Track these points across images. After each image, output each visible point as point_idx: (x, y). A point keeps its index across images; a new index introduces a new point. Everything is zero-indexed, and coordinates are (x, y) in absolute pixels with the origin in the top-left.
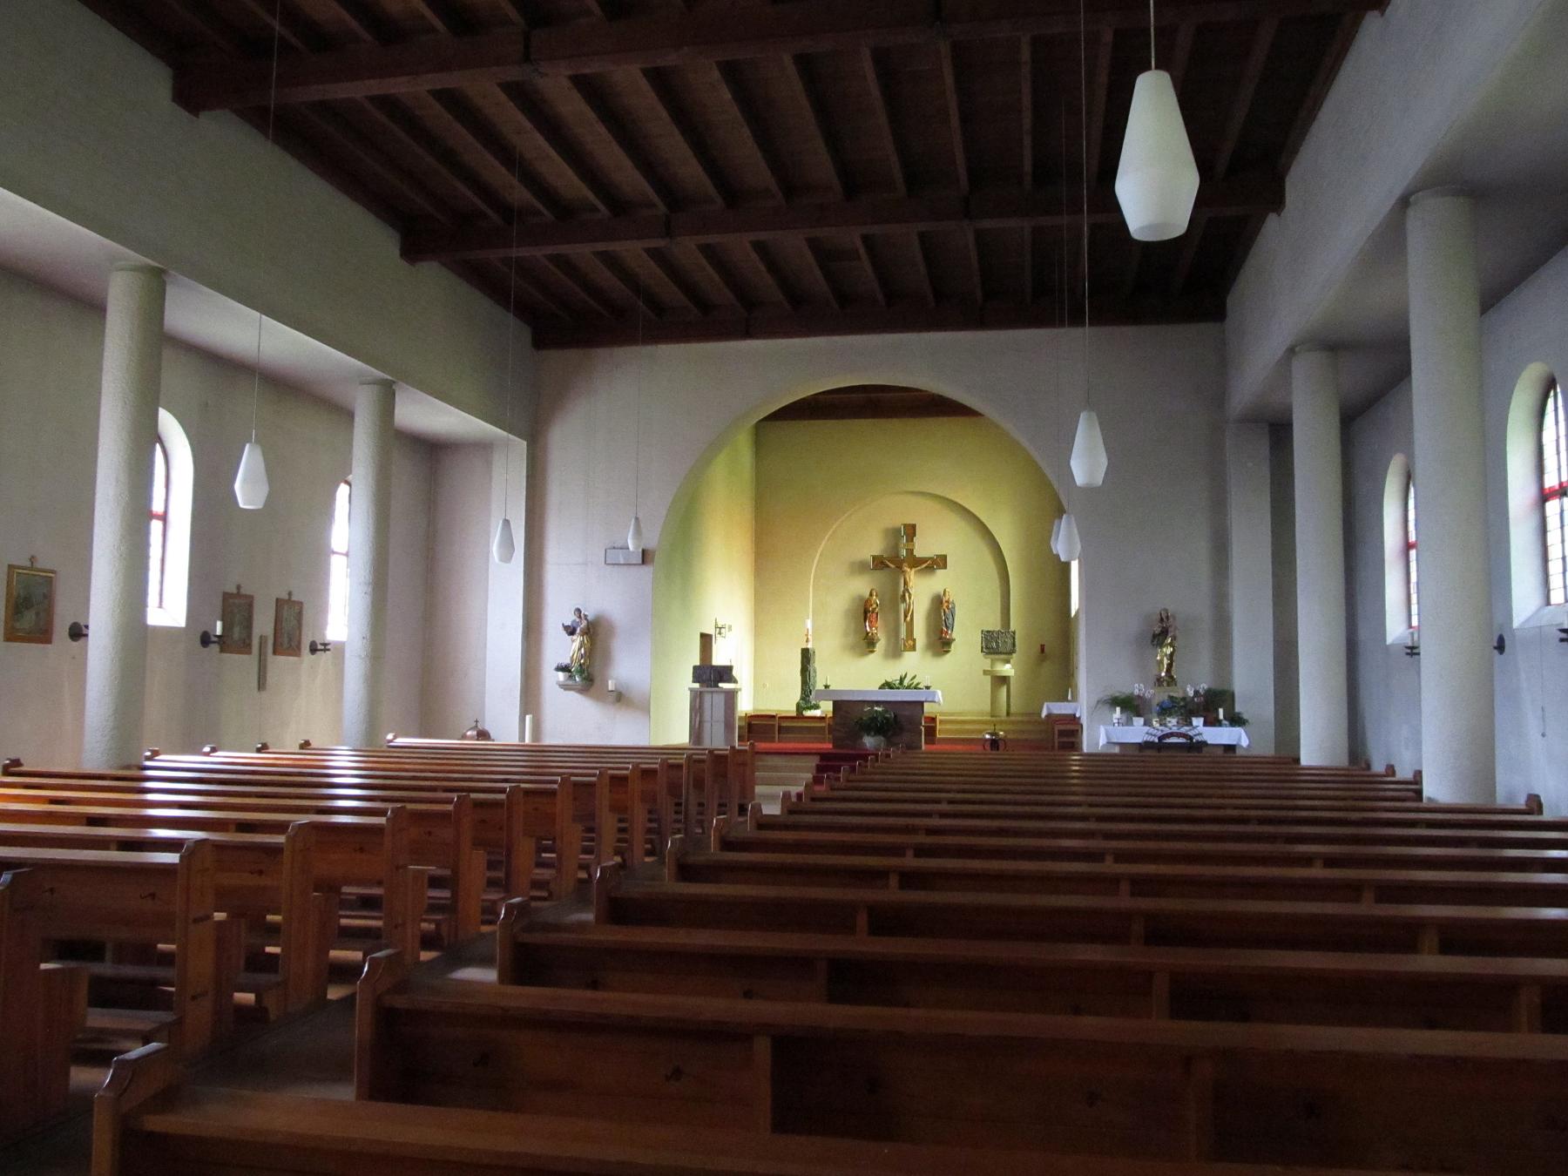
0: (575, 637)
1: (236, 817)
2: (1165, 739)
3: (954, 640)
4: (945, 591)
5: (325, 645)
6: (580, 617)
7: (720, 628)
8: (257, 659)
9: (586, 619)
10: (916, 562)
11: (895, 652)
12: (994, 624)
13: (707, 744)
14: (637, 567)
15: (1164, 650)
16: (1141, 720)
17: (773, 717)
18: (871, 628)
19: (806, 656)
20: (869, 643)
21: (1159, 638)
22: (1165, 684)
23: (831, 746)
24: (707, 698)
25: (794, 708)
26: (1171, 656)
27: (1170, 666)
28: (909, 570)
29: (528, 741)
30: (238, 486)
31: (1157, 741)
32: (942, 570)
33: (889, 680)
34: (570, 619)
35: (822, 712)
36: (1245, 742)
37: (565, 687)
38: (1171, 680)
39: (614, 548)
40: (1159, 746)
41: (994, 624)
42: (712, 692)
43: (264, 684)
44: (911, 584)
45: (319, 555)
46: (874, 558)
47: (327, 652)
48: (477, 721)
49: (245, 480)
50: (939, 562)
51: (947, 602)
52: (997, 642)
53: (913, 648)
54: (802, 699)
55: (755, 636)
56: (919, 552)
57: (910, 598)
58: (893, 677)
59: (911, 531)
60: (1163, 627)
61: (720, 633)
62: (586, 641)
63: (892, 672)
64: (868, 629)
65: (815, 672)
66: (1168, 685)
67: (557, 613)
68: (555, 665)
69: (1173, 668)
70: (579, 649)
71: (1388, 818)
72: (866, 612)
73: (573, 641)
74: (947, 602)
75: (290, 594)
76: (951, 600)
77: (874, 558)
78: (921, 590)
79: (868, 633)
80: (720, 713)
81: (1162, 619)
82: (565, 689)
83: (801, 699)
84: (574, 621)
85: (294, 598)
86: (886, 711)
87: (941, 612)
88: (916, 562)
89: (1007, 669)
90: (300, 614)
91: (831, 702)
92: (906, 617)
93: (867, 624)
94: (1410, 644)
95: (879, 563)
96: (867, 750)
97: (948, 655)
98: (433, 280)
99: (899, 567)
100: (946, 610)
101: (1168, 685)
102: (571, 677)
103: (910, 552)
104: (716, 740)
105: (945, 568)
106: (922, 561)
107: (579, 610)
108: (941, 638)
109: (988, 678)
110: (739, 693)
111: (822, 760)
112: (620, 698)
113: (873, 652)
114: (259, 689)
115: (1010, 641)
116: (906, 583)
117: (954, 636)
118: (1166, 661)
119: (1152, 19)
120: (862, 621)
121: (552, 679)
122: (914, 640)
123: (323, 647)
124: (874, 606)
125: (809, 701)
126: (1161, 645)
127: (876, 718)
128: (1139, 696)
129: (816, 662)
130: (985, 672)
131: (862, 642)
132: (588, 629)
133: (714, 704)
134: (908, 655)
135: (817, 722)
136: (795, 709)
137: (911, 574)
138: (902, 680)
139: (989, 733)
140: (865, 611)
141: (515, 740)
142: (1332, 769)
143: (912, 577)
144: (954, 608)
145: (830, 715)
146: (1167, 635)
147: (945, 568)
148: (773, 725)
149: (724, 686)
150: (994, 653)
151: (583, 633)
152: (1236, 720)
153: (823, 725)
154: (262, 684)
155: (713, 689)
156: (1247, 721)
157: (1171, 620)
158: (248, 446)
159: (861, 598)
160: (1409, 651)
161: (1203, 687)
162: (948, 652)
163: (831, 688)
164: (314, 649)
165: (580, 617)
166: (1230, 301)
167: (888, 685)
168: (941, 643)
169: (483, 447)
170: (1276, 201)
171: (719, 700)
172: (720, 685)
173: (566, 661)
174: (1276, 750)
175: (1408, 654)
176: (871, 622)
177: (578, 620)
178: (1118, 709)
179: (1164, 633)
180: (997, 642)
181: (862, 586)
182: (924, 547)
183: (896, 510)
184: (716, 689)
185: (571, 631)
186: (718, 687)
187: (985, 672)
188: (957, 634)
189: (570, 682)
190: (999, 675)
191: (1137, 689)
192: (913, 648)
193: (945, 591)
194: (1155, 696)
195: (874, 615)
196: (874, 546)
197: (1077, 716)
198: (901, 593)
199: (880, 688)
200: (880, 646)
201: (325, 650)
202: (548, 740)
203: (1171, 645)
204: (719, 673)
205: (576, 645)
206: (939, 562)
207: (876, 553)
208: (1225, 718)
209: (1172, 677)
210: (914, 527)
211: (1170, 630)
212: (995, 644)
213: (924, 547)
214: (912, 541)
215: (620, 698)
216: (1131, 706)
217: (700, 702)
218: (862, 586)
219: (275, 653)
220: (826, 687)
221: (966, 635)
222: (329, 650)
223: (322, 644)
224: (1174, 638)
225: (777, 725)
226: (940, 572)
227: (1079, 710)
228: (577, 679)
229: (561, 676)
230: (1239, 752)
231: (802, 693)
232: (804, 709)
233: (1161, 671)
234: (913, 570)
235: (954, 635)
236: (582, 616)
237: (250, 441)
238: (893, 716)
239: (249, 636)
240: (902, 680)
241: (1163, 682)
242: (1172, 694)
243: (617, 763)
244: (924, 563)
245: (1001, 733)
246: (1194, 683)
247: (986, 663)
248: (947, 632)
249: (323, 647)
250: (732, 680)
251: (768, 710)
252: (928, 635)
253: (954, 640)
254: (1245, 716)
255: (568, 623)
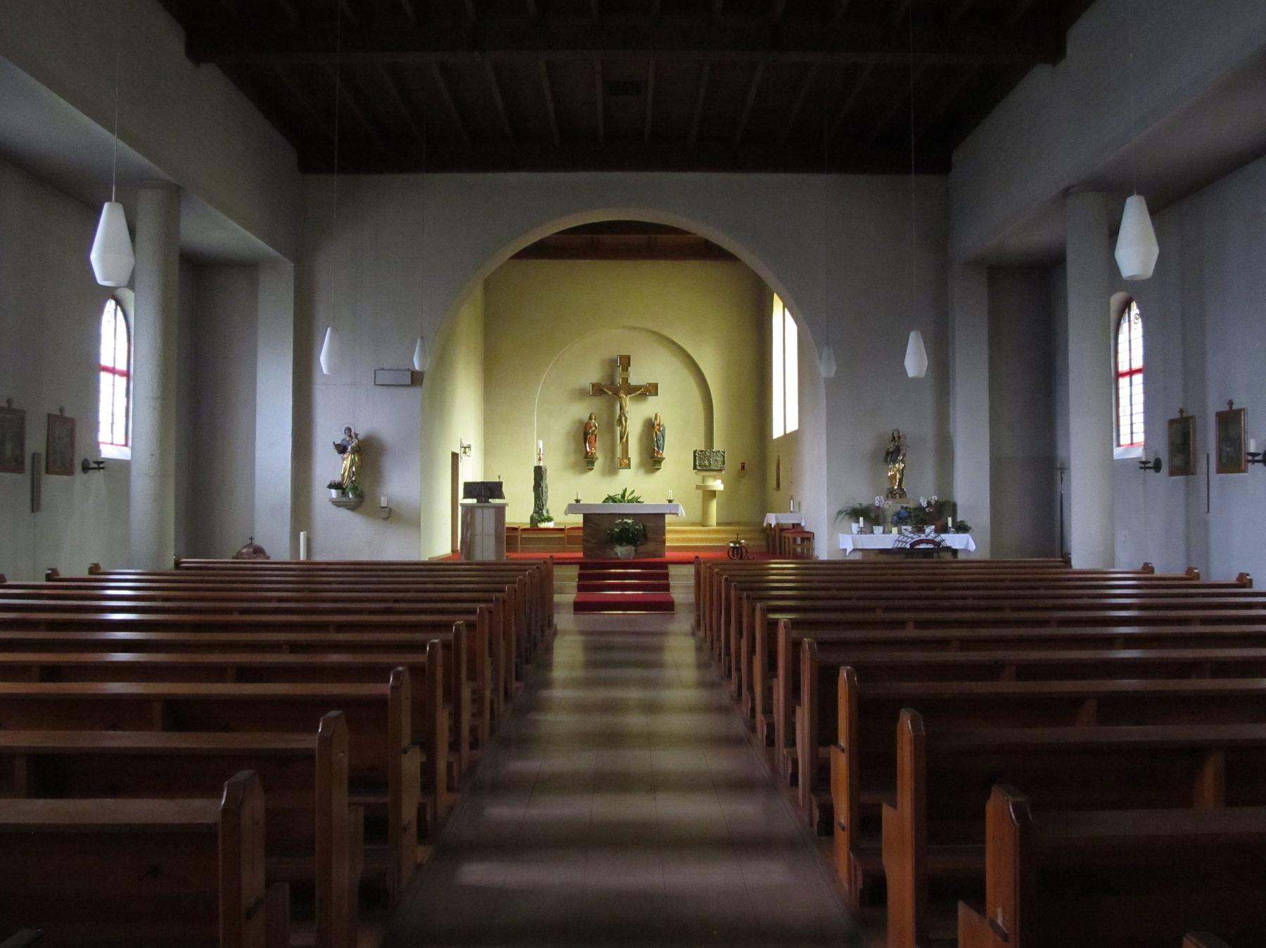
0: (345, 456)
1: (192, 692)
2: (915, 545)
3: (664, 459)
4: (656, 415)
5: (99, 463)
6: (350, 436)
7: (465, 448)
8: (30, 477)
9: (356, 438)
10: (631, 390)
11: (612, 469)
12: (701, 446)
13: (478, 557)
14: (402, 389)
15: (897, 465)
16: (881, 528)
17: (515, 529)
18: (590, 448)
19: (539, 473)
20: (588, 462)
21: (892, 455)
22: (897, 496)
23: (581, 555)
24: (478, 513)
25: (528, 521)
26: (902, 472)
27: (901, 480)
28: (625, 396)
29: (302, 557)
30: (94, 256)
31: (908, 546)
32: (654, 397)
33: (611, 495)
34: (340, 438)
35: (555, 524)
36: (972, 547)
37: (337, 503)
38: (902, 493)
39: (383, 369)
40: (912, 552)
41: (701, 446)
42: (483, 507)
43: (39, 504)
44: (627, 409)
45: (90, 368)
46: (593, 385)
47: (101, 470)
48: (252, 539)
49: (106, 249)
50: (652, 390)
51: (659, 425)
52: (709, 461)
53: (628, 466)
54: (535, 512)
55: (485, 453)
56: (634, 380)
57: (626, 421)
58: (616, 491)
59: (626, 362)
60: (896, 446)
61: (465, 452)
62: (357, 459)
63: (614, 486)
64: (588, 449)
65: (546, 488)
66: (900, 497)
67: (327, 432)
68: (328, 483)
69: (903, 482)
70: (351, 467)
71: (1219, 616)
72: (586, 434)
73: (344, 459)
74: (659, 425)
75: (61, 410)
76: (661, 424)
77: (593, 385)
78: (636, 414)
79: (587, 453)
80: (490, 527)
81: (894, 438)
82: (339, 506)
83: (534, 513)
84: (344, 440)
85: (67, 414)
86: (635, 523)
87: (653, 434)
88: (631, 390)
89: (717, 485)
90: (72, 433)
91: (582, 515)
92: (622, 438)
93: (587, 445)
94: (1144, 459)
95: (598, 390)
96: (618, 558)
97: (658, 473)
98: (211, 78)
99: (616, 393)
100: (658, 432)
101: (900, 497)
102: (344, 493)
103: (626, 380)
104: (486, 551)
105: (656, 394)
106: (637, 388)
107: (349, 430)
108: (652, 457)
109: (700, 492)
110: (507, 508)
111: (581, 569)
112: (389, 515)
113: (592, 469)
114: (33, 511)
115: (720, 459)
116: (621, 408)
117: (664, 456)
118: (898, 476)
119: (113, 195)
120: (583, 441)
121: (323, 496)
122: (629, 459)
123: (96, 466)
124: (594, 428)
125: (542, 514)
126: (895, 461)
127: (628, 530)
128: (879, 507)
129: (548, 479)
130: (698, 487)
131: (649, 459)
132: (359, 447)
133: (485, 522)
134: (624, 473)
135: (552, 533)
136: (529, 521)
137: (627, 400)
138: (623, 496)
139: (731, 542)
140: (585, 434)
141: (286, 557)
142: (980, 562)
143: (628, 403)
144: (664, 430)
145: (582, 525)
146: (899, 452)
147: (656, 394)
148: (517, 537)
149: (497, 501)
150: (705, 470)
151: (354, 451)
152: (961, 528)
153: (562, 535)
154: (35, 505)
155: (485, 504)
156: (970, 528)
157: (902, 439)
158: (106, 206)
159: (580, 422)
160: (1142, 465)
161: (934, 498)
162: (659, 469)
163: (581, 502)
164: (86, 468)
165: (350, 436)
166: (957, 156)
167: (611, 499)
168: (652, 461)
169: (247, 267)
170: (1054, 52)
171: (490, 515)
172: (490, 500)
173: (338, 479)
174: (991, 554)
175: (1141, 468)
176: (590, 443)
177: (348, 439)
178: (861, 519)
179: (897, 451)
180: (709, 461)
181: (581, 410)
182: (637, 377)
183: (612, 342)
184: (488, 504)
185: (341, 449)
186: (488, 502)
187: (698, 487)
188: (667, 453)
189: (344, 499)
190: (710, 489)
191: (879, 500)
192: (628, 466)
193: (656, 415)
194: (891, 506)
195: (594, 436)
196: (592, 374)
197: (803, 524)
198: (618, 417)
199: (604, 502)
200: (598, 464)
201: (99, 468)
202: (318, 557)
203: (903, 461)
204: (490, 489)
205: (347, 463)
206: (652, 390)
207: (595, 381)
208: (953, 526)
209: (902, 490)
210: (628, 358)
211: (901, 448)
212: (702, 462)
213: (637, 377)
214: (627, 370)
215: (389, 515)
216: (869, 516)
217: (471, 518)
218: (581, 410)
219: (48, 472)
220: (578, 501)
221: (677, 454)
222: (103, 468)
223: (95, 462)
224: (904, 455)
225: (519, 537)
226: (651, 399)
227: (803, 521)
228: (351, 496)
229: (334, 493)
230: (961, 556)
231: (535, 507)
232: (539, 521)
233: (893, 484)
234: (629, 396)
235: (664, 455)
236: (353, 435)
237: (110, 200)
238: (642, 527)
239: (22, 455)
240: (623, 496)
241: (895, 494)
242: (905, 505)
243: (410, 576)
244: (638, 390)
245: (743, 541)
246: (925, 496)
247: (696, 478)
248: (658, 452)
249: (96, 466)
250: (501, 496)
251: (514, 523)
252: (641, 454)
253: (664, 459)
254: (969, 524)
255: (338, 442)
